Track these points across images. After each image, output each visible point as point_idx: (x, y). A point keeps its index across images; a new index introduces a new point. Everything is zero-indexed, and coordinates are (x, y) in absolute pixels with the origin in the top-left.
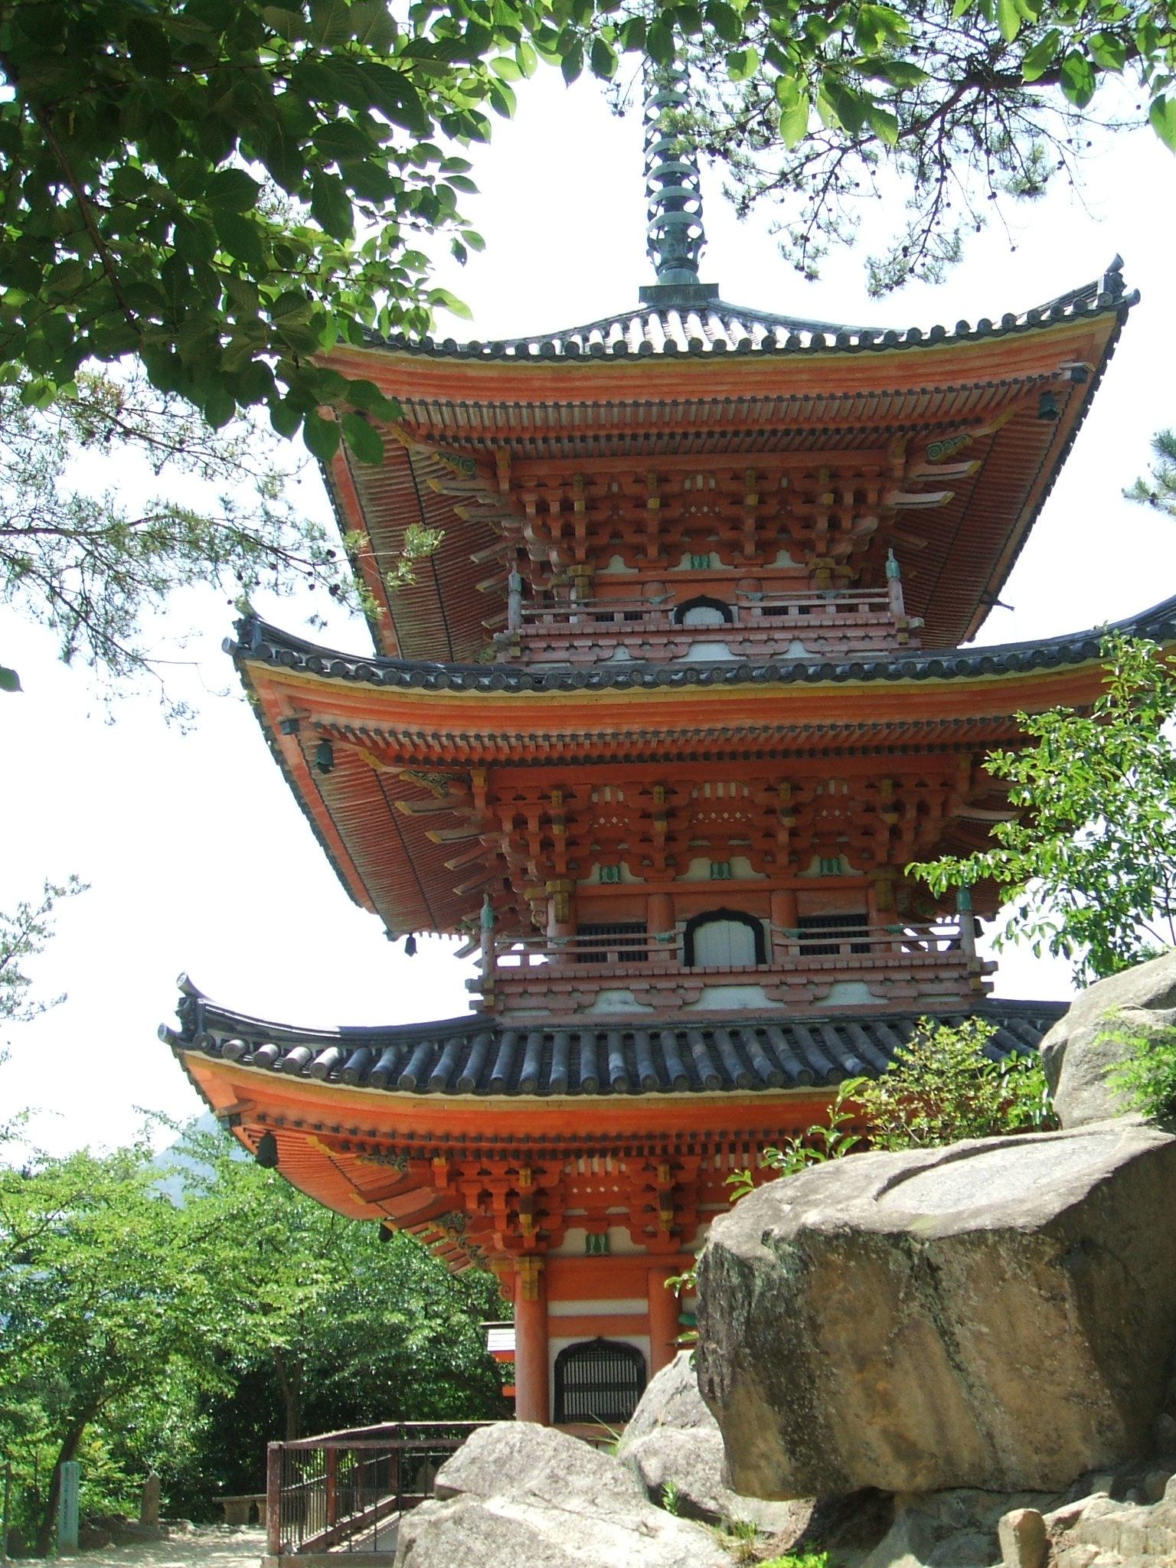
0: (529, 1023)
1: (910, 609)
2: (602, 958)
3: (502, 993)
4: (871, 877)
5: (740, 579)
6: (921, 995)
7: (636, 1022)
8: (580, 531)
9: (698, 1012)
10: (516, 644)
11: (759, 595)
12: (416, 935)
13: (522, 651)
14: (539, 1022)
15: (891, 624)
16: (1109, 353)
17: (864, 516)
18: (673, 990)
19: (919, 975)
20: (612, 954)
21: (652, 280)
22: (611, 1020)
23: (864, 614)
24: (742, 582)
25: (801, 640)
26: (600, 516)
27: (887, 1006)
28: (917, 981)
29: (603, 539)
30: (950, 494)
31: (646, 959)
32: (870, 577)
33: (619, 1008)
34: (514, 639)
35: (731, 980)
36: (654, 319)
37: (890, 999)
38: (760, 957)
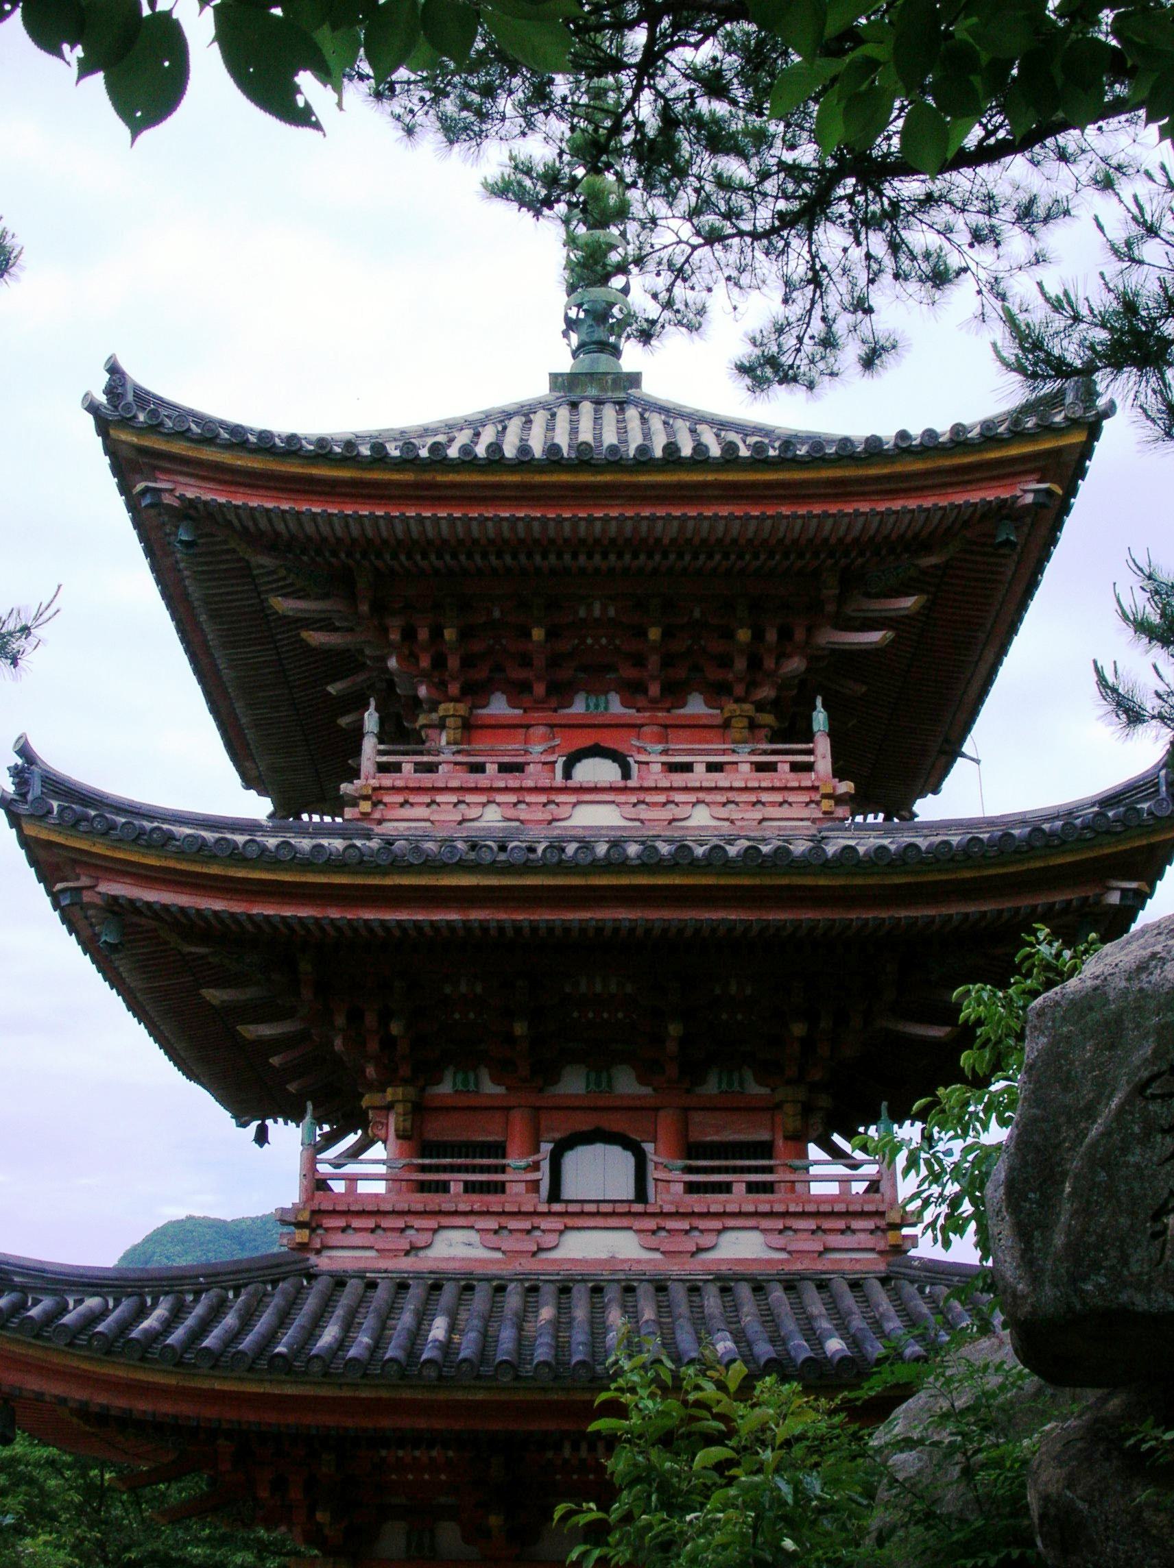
0: (350, 1266)
1: (839, 773)
2: (443, 1187)
3: (320, 1226)
4: (778, 1097)
5: (642, 725)
6: (827, 1250)
7: (479, 1271)
8: (453, 663)
9: (555, 1260)
10: (366, 798)
11: (660, 747)
12: (269, 1122)
13: (375, 805)
14: (362, 1265)
15: (815, 788)
16: (1081, 473)
17: (790, 656)
18: (528, 1232)
19: (827, 1224)
20: (456, 1183)
21: (565, 364)
22: (451, 1266)
23: (783, 774)
24: (645, 729)
25: (707, 804)
26: (478, 646)
27: (787, 1261)
28: (825, 1231)
29: (481, 674)
30: (890, 634)
31: (503, 1191)
32: (795, 730)
33: (461, 1252)
34: (364, 792)
35: (600, 1222)
36: (563, 413)
37: (789, 1252)
38: (641, 1194)
